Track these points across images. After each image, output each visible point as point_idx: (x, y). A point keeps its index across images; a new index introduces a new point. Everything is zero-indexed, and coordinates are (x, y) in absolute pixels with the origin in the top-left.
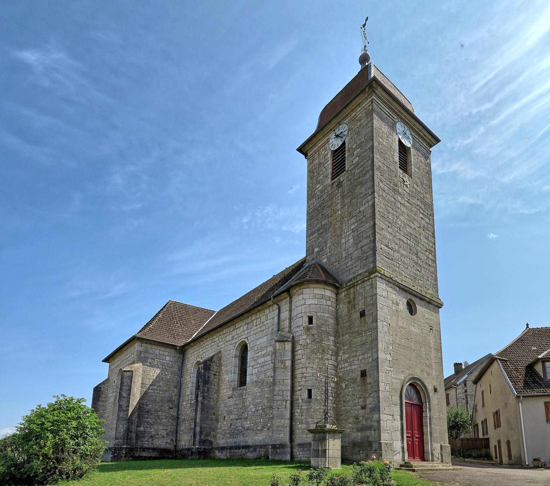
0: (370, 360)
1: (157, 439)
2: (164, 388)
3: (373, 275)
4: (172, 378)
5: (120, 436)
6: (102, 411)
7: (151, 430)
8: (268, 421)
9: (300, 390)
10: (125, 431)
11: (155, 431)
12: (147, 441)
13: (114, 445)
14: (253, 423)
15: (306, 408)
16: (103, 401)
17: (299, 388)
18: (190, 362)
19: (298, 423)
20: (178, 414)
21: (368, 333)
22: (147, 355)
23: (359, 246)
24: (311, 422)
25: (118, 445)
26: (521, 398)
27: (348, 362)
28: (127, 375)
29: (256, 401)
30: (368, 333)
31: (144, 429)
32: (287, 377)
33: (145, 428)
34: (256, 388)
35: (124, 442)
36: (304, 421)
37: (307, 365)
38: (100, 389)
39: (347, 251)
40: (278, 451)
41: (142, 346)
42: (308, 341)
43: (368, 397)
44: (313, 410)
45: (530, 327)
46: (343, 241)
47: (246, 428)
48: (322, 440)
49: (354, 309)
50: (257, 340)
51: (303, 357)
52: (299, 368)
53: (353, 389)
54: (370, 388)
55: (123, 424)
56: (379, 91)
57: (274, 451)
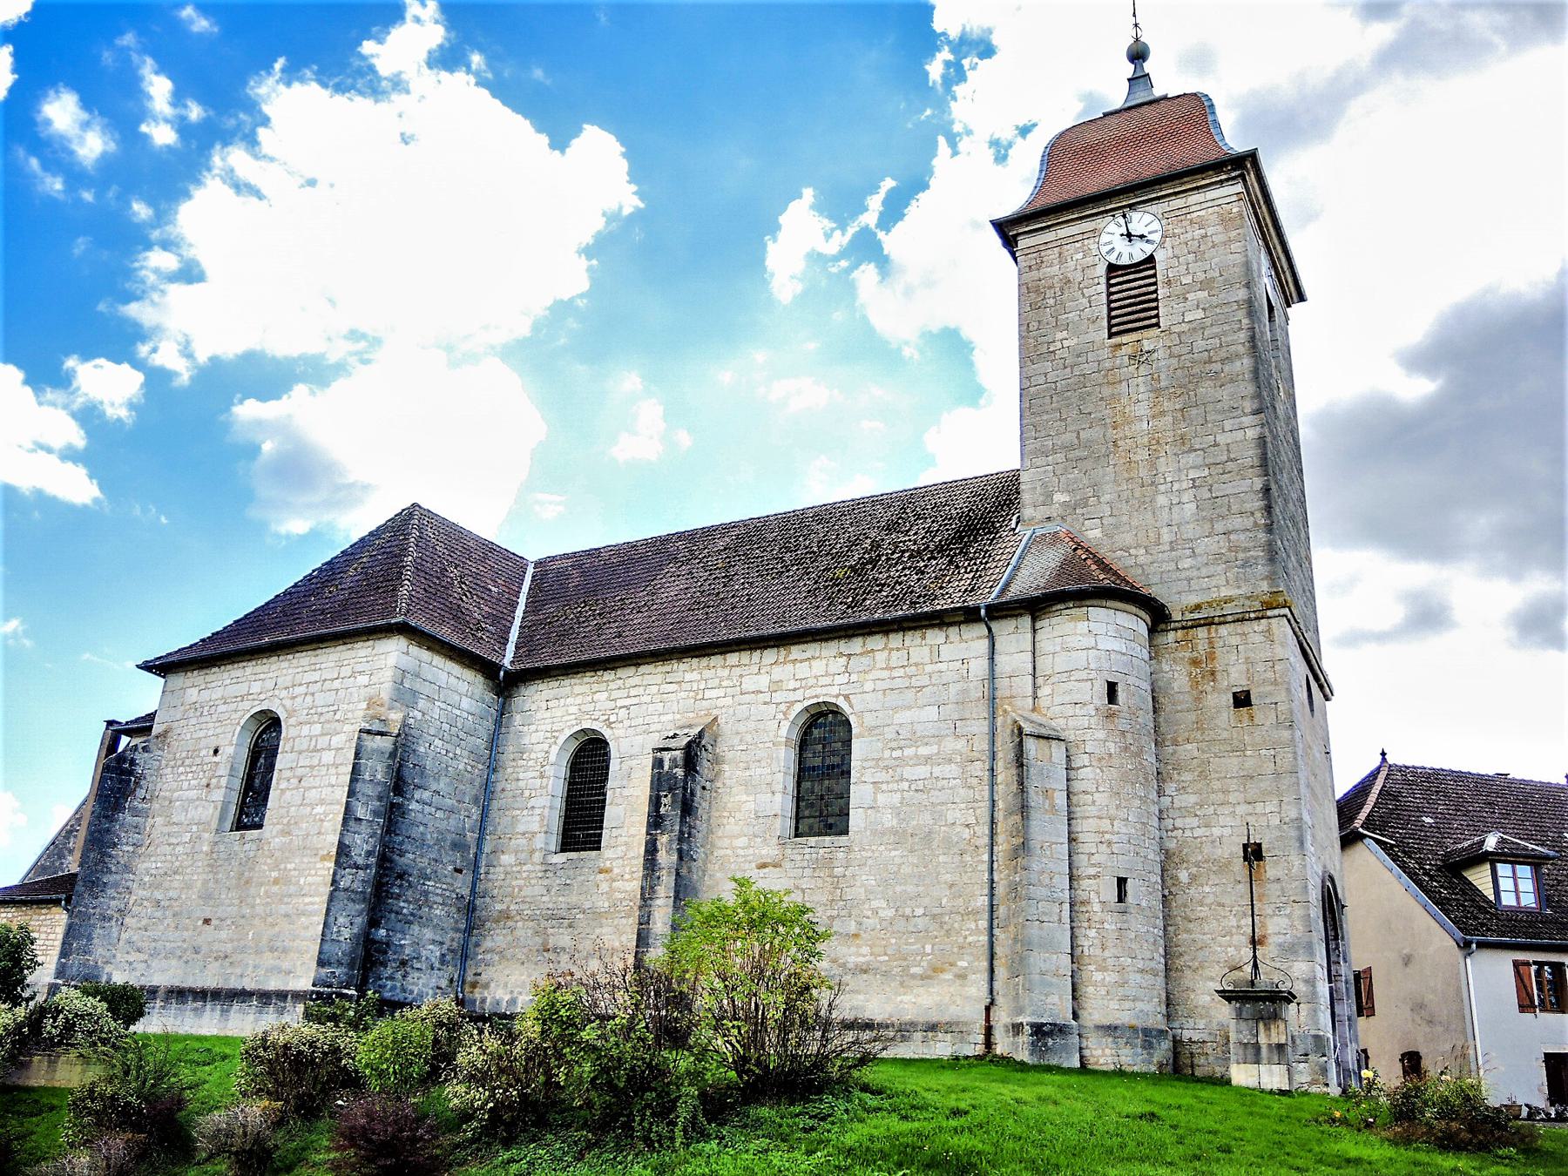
0: (1275, 821)
1: (416, 975)
2: (449, 801)
3: (1276, 612)
4: (469, 768)
5: (337, 954)
6: (131, 849)
7: (403, 942)
8: (958, 954)
9: (1095, 877)
10: (357, 936)
11: (411, 945)
12: (391, 978)
13: (314, 985)
14: (886, 954)
15: (1114, 927)
16: (136, 813)
17: (1092, 871)
18: (543, 727)
19: (1092, 968)
20: (473, 891)
21: (1263, 752)
22: (418, 686)
23: (1220, 527)
24: (1130, 968)
25: (328, 987)
26: (1474, 946)
27: (1196, 815)
28: (375, 746)
29: (898, 889)
30: (1263, 752)
31: (388, 936)
32: (1059, 836)
33: (391, 933)
34: (895, 850)
35: (351, 977)
36: (1110, 962)
37: (1113, 812)
38: (131, 765)
39: (1175, 529)
40: (1050, 1042)
41: (408, 654)
42: (1112, 748)
43: (1271, 916)
44: (1133, 935)
45: (1391, 759)
46: (1162, 500)
47: (850, 966)
48: (1269, 1019)
49: (1213, 681)
50: (895, 709)
51: (1101, 789)
52: (1087, 815)
53: (1218, 889)
54: (1279, 893)
55: (353, 913)
56: (1251, 178)
57: (1039, 1040)
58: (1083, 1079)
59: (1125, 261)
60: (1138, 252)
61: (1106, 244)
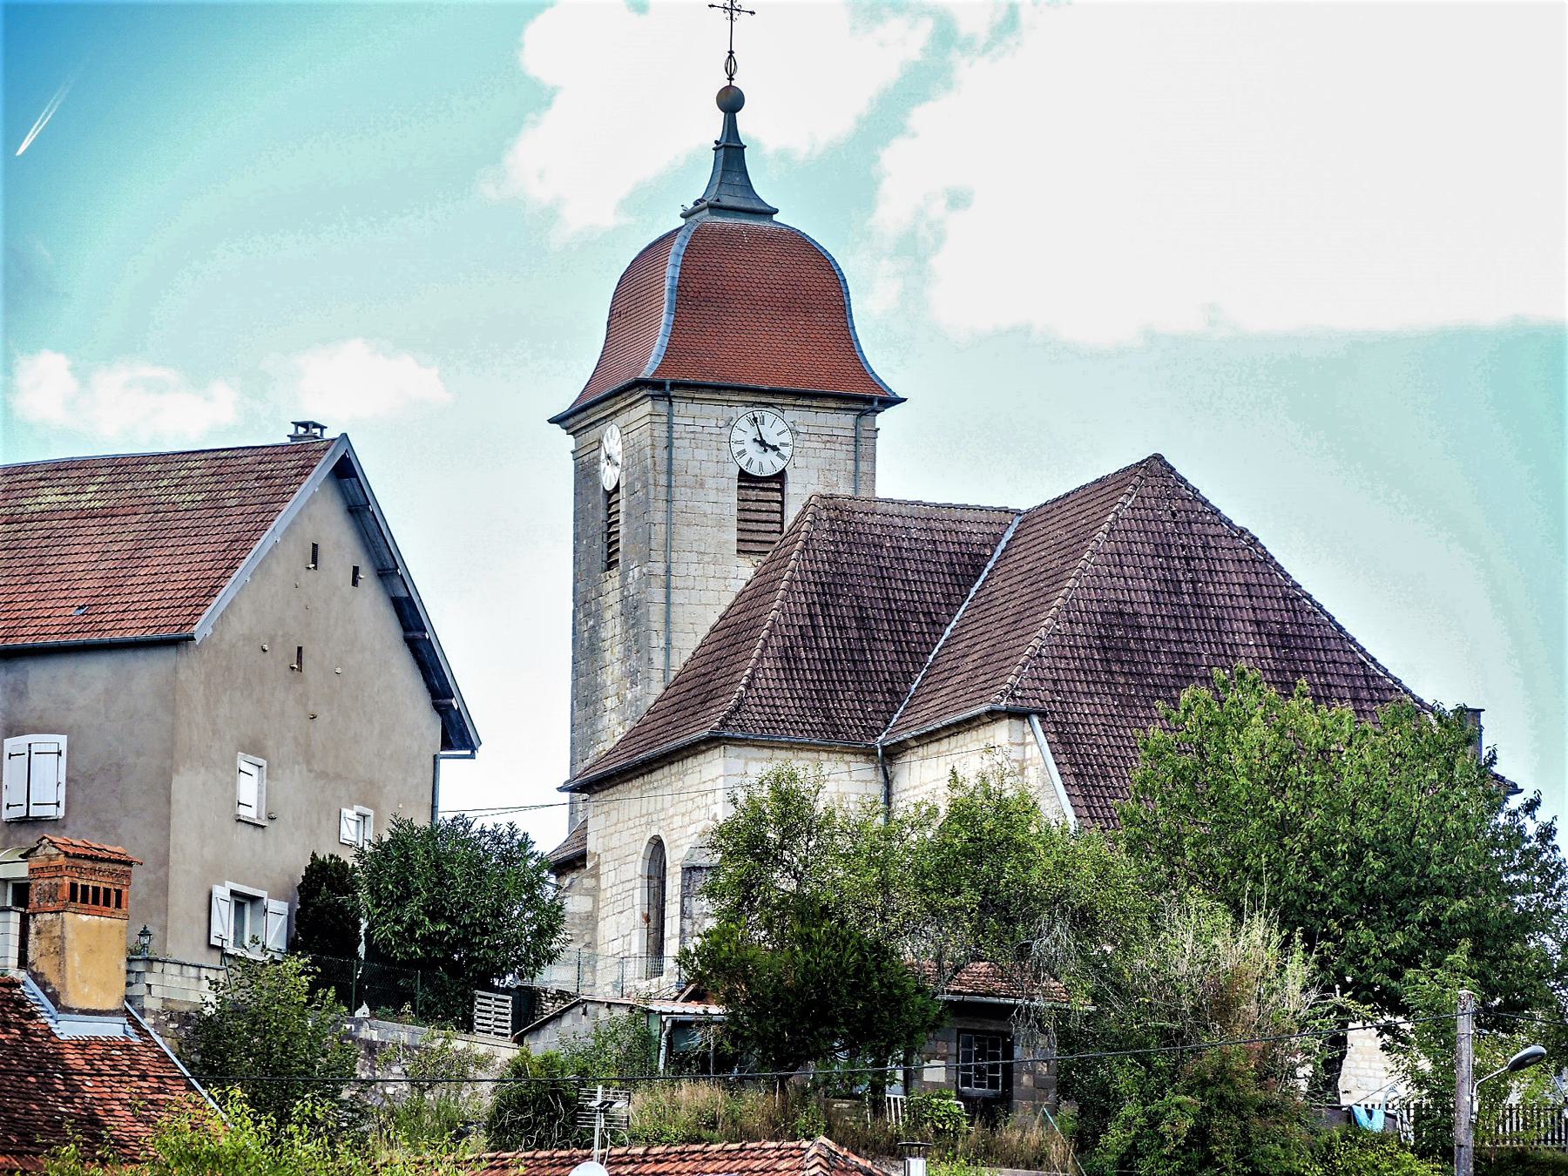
59: (754, 470)
60: (766, 465)
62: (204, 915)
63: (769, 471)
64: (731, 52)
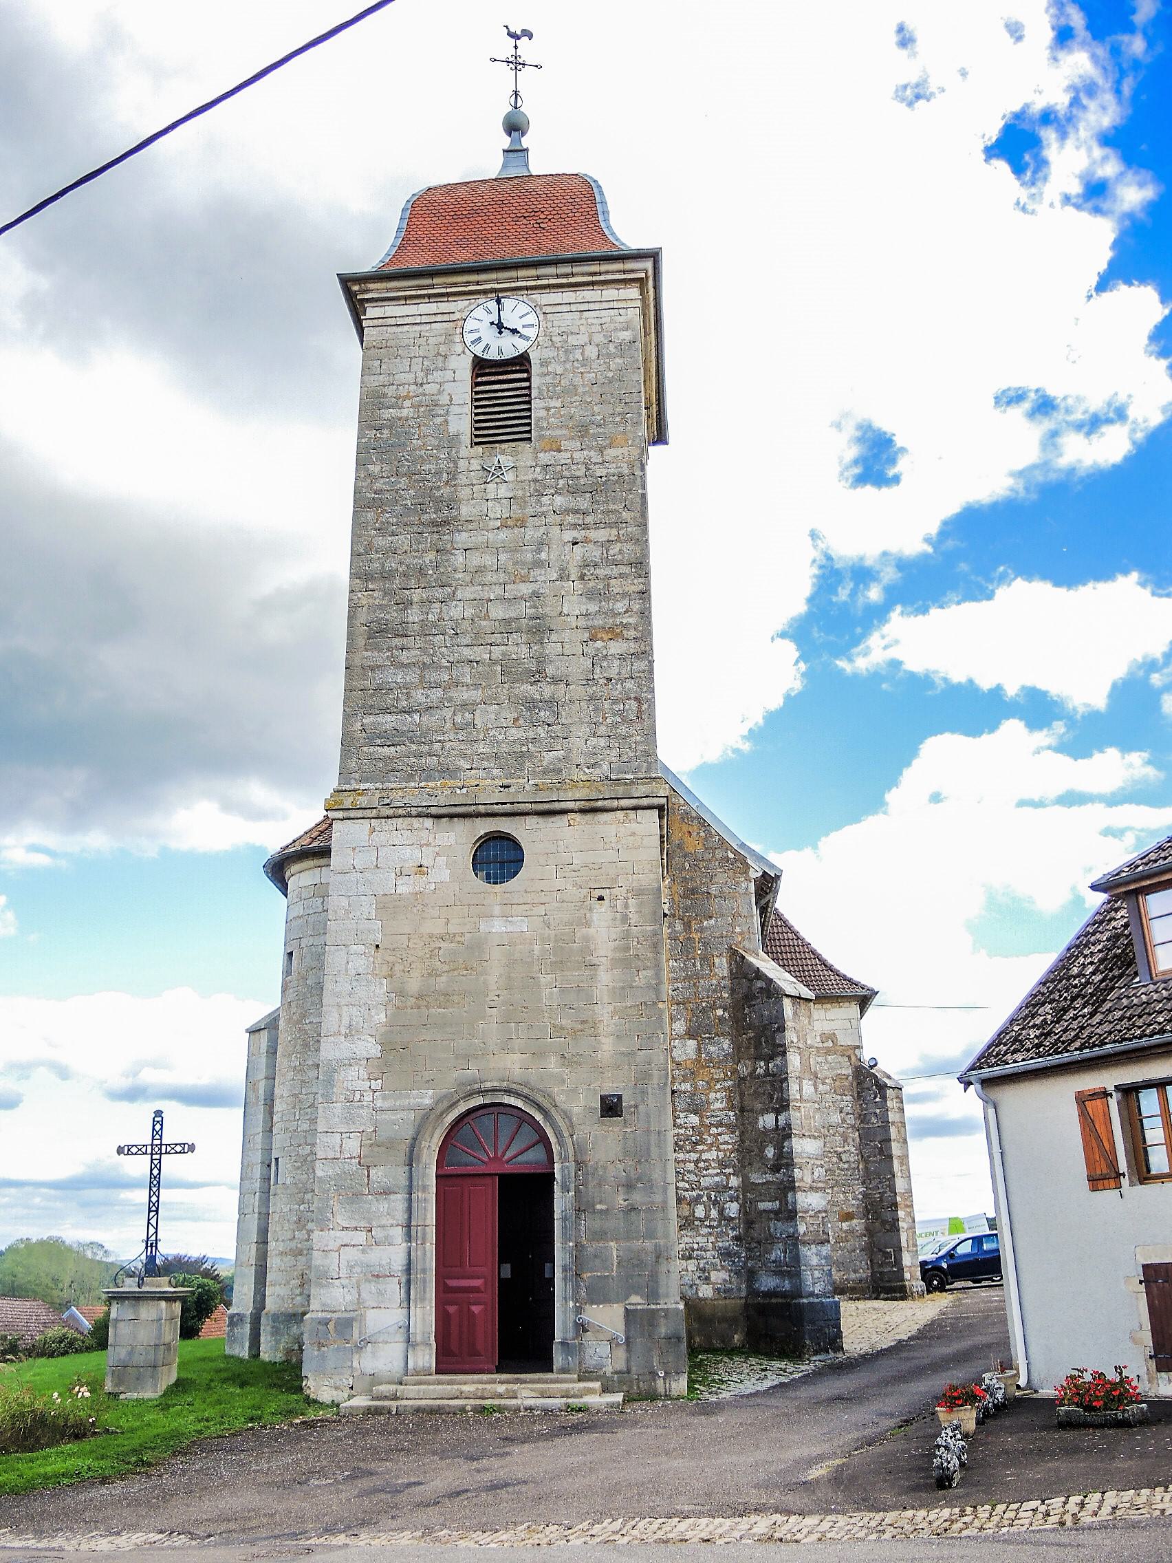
58: (547, 851)
59: (492, 355)
60: (509, 347)
61: (471, 332)
62: (1029, 1339)
63: (509, 353)
64: (516, 93)
